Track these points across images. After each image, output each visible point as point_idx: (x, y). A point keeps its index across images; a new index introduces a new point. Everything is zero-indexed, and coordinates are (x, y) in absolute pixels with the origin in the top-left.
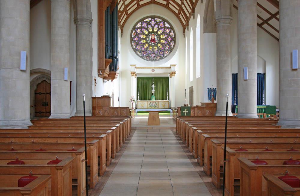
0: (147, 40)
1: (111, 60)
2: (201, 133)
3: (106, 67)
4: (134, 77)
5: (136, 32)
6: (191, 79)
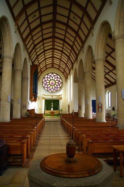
1: (35, 94)
2: (75, 129)
6: (69, 101)
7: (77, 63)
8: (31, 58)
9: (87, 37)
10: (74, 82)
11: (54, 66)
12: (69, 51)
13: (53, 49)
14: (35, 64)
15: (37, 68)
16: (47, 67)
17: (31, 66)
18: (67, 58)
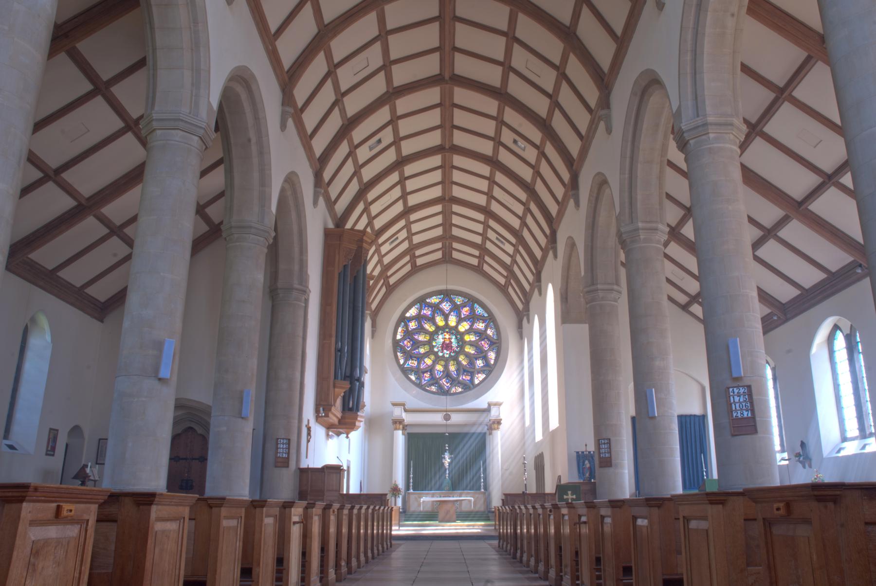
0: (434, 347)
3: (335, 401)
4: (400, 432)
6: (539, 436)
7: (555, 256)
8: (300, 126)
9: (586, 140)
11: (456, 255)
13: (447, 149)
14: (352, 229)
15: (360, 248)
17: (327, 233)
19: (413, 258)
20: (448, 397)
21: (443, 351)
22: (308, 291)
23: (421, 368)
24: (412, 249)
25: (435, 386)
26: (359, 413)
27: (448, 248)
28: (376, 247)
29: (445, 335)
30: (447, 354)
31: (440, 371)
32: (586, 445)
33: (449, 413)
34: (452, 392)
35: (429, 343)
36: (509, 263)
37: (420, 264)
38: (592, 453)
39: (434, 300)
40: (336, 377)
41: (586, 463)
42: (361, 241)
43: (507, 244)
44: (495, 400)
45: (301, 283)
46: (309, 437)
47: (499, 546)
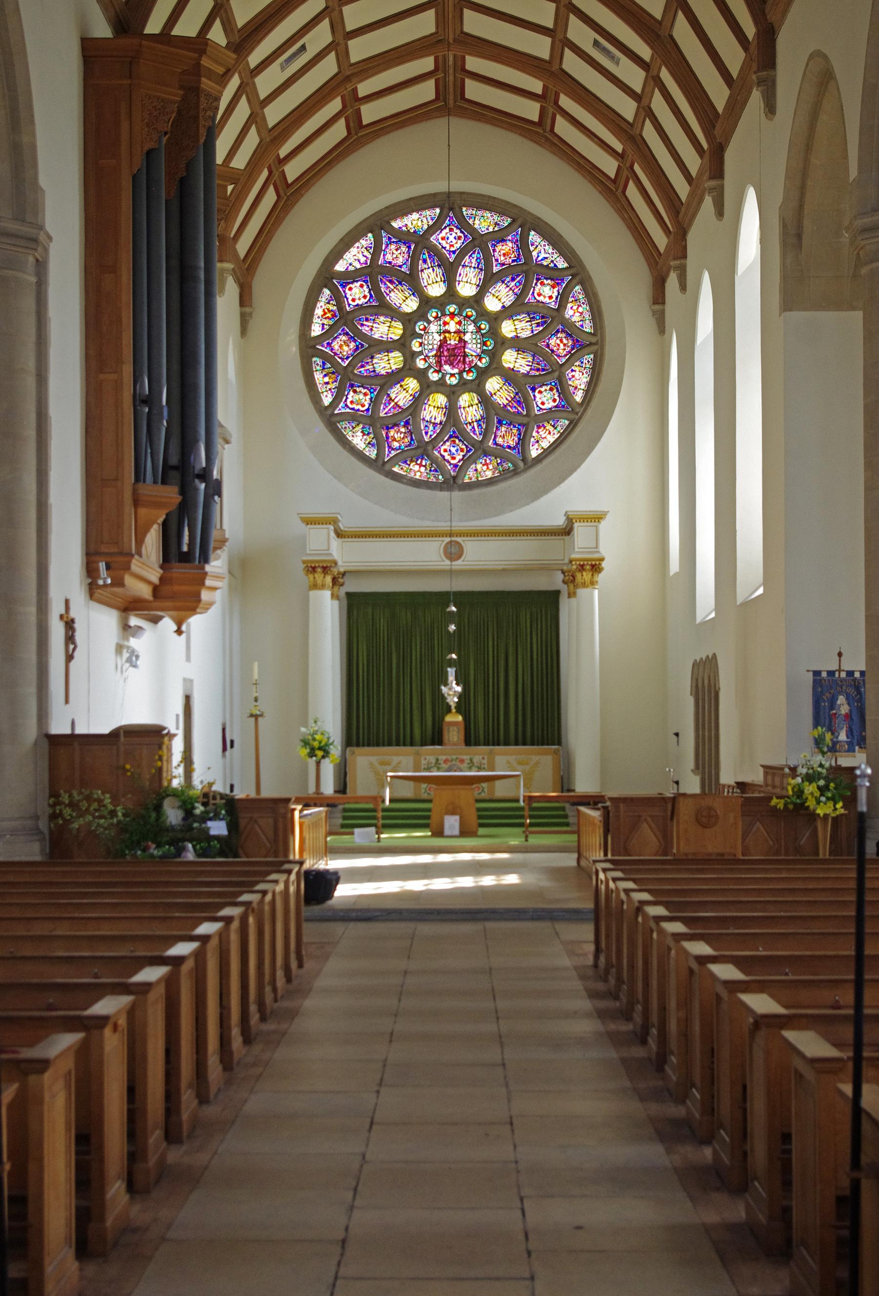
0: (414, 355)
3: (140, 542)
5: (338, 298)
7: (771, 108)
10: (788, 305)
11: (474, 91)
12: (635, 77)
14: (165, 36)
16: (370, 113)
18: (619, 147)
19: (353, 102)
20: (457, 494)
21: (441, 366)
22: (42, 237)
23: (382, 414)
24: (348, 79)
25: (421, 465)
26: (208, 568)
27: (451, 71)
28: (241, 77)
29: (445, 323)
30: (452, 375)
31: (435, 425)
32: (840, 655)
33: (459, 539)
34: (466, 480)
35: (402, 345)
36: (630, 118)
37: (368, 122)
38: (857, 675)
39: (415, 222)
40: (139, 476)
41: (839, 702)
42: (197, 70)
43: (624, 59)
44: (581, 505)
45: (20, 217)
46: (71, 647)
47: (596, 966)
